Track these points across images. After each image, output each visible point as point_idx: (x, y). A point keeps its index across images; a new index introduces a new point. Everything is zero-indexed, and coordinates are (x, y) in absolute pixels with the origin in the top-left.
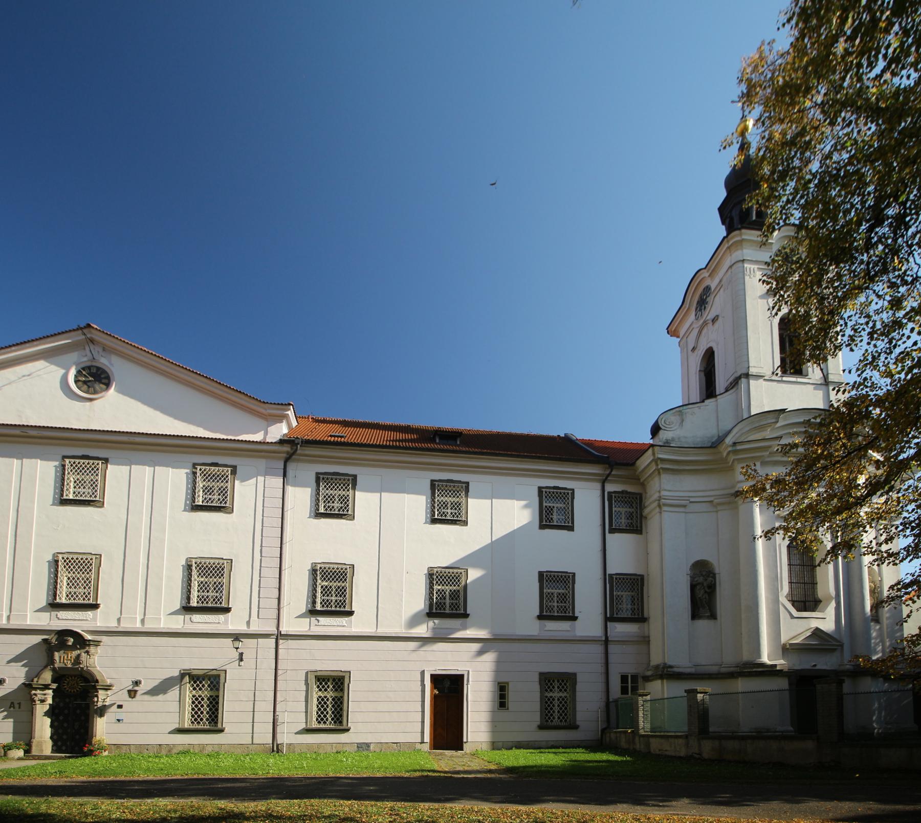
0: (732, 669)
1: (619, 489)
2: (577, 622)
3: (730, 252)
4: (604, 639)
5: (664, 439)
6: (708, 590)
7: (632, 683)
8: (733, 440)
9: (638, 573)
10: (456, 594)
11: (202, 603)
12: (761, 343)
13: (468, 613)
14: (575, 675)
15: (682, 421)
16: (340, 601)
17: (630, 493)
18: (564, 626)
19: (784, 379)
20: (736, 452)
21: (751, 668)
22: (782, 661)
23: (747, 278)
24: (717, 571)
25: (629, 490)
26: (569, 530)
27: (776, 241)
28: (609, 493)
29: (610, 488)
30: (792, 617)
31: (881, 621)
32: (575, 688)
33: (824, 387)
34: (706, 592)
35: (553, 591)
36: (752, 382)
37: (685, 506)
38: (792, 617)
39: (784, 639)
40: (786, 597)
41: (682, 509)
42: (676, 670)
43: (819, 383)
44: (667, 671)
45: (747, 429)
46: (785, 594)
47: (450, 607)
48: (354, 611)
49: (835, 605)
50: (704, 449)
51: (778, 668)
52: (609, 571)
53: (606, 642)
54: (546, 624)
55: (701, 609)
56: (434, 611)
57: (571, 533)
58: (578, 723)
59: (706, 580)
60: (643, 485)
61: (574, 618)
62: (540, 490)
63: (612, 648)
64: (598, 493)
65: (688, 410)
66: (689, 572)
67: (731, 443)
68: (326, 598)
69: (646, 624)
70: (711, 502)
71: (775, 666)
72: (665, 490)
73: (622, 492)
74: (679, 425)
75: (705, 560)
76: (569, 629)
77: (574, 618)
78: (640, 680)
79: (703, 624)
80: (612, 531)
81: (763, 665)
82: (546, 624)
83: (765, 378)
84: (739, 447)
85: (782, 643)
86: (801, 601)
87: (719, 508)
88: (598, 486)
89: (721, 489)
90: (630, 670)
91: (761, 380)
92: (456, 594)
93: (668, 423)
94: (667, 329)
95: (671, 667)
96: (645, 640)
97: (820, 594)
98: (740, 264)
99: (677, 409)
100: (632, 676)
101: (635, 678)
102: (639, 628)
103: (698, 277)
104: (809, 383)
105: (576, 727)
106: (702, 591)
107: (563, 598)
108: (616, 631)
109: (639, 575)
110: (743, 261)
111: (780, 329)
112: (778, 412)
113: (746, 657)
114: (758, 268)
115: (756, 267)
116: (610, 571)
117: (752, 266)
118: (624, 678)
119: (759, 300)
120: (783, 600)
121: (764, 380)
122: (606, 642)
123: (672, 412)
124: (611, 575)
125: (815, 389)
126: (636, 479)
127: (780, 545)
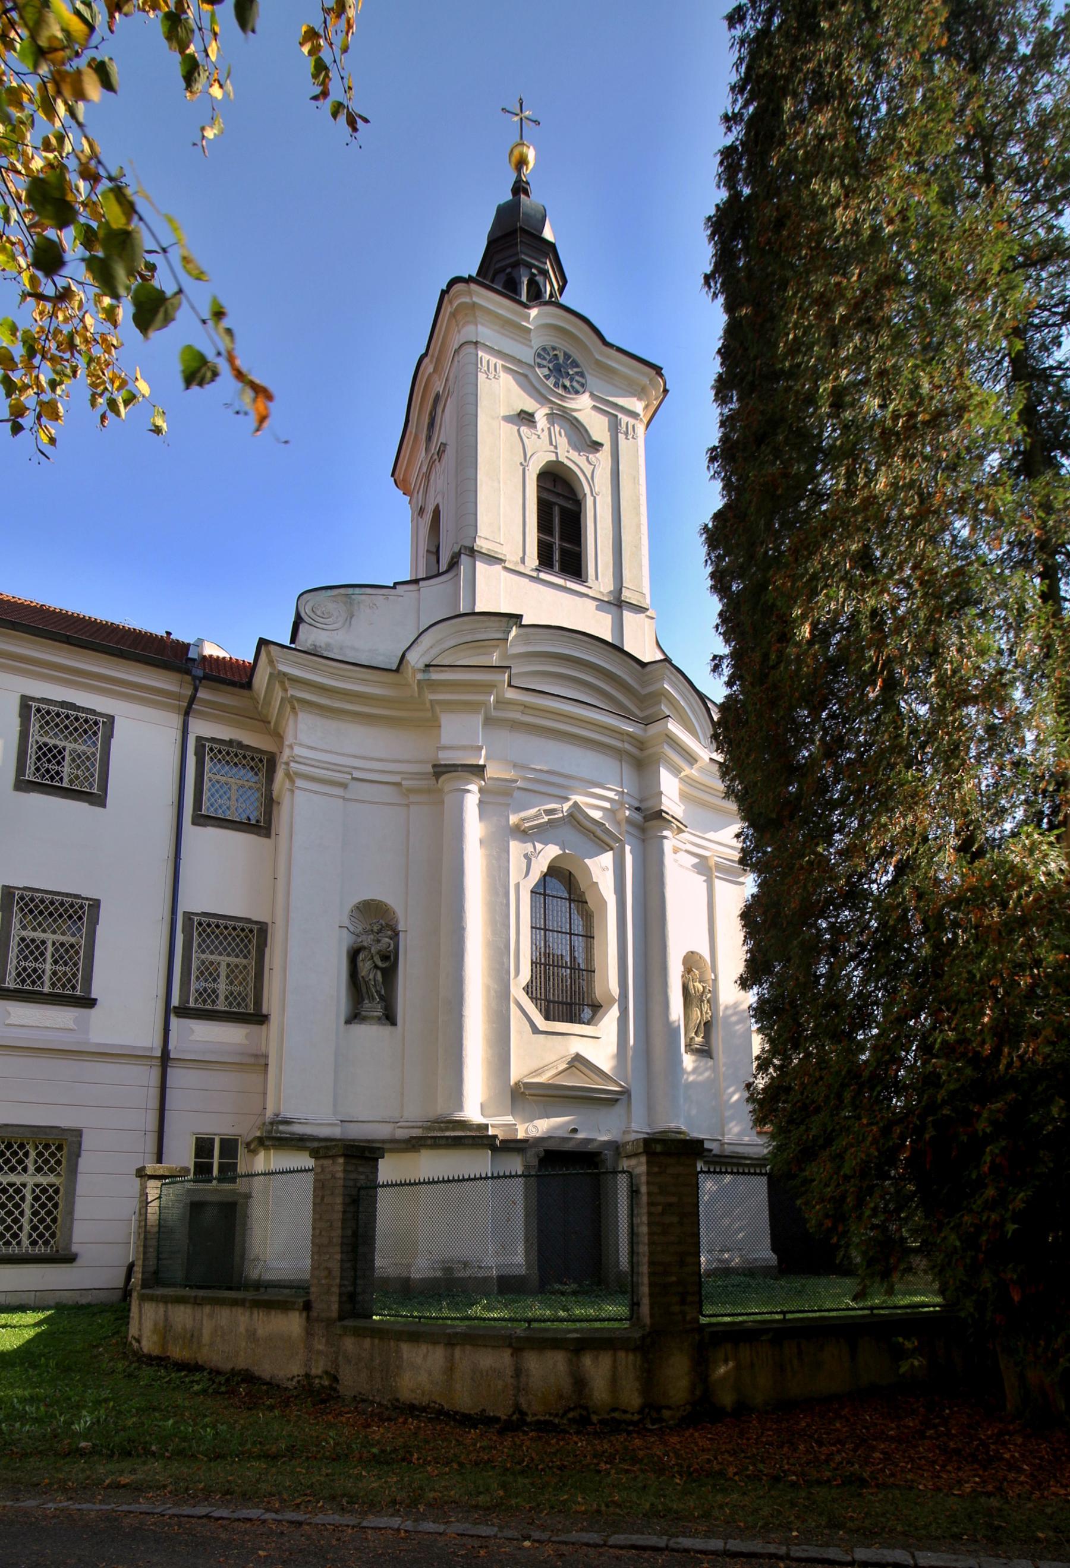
0: (417, 1133)
1: (226, 737)
2: (93, 1012)
3: (457, 325)
4: (159, 1054)
5: (310, 642)
6: (380, 964)
7: (221, 1157)
8: (426, 660)
9: (255, 919)
10: (37, 947)
11: (205, 1001)
12: (502, 500)
13: (93, 996)
14: (78, 1133)
15: (352, 616)
16: (65, 974)
17: (248, 747)
18: (61, 1017)
19: (542, 576)
20: (433, 685)
21: (441, 1130)
22: (510, 1118)
23: (481, 377)
24: (401, 927)
25: (246, 742)
26: (92, 803)
27: (537, 328)
28: (199, 739)
29: (200, 728)
30: (535, 1030)
31: (714, 1055)
32: (76, 1165)
33: (614, 609)
34: (376, 967)
35: (43, 936)
36: (480, 566)
37: (344, 786)
38: (535, 1030)
39: (517, 1073)
40: (527, 989)
41: (338, 791)
42: (298, 1129)
43: (606, 599)
44: (277, 1131)
45: (453, 643)
46: (524, 984)
47: (227, 998)
48: (96, 1000)
49: (618, 1014)
50: (385, 673)
51: (491, 1132)
52: (183, 907)
53: (165, 1059)
54: (193, 1026)
55: (366, 1001)
56: (192, 1004)
57: (98, 810)
58: (75, 1248)
59: (378, 941)
60: (278, 736)
61: (90, 1003)
62: (25, 704)
63: (175, 1075)
64: (173, 734)
65: (363, 597)
66: (346, 922)
67: (421, 665)
68: (30, 964)
69: (264, 1027)
70: (398, 784)
71: (486, 1127)
72: (301, 745)
73: (231, 742)
74: (344, 624)
75: (372, 900)
76: (72, 1026)
77: (90, 1003)
78: (241, 1150)
79: (369, 1033)
80: (201, 819)
81: (463, 1124)
82: (193, 1026)
83: (507, 565)
84: (436, 676)
85: (512, 1083)
86: (562, 1003)
87: (413, 798)
88: (176, 720)
89: (416, 762)
90: (218, 1127)
91: (498, 568)
92: (37, 947)
93: (319, 613)
94: (393, 475)
95: (287, 1122)
96: (258, 1063)
97: (599, 994)
98: (470, 349)
99: (342, 591)
100: (222, 1141)
101: (229, 1147)
102: (247, 1036)
103: (423, 374)
104: (587, 596)
105: (70, 1259)
106: (368, 964)
107: (65, 953)
108: (192, 1038)
109: (257, 923)
110: (476, 343)
111: (540, 488)
112: (505, 619)
113: (440, 1108)
114: (503, 366)
115: (500, 363)
116: (189, 903)
117: (493, 360)
118: (203, 1147)
119: (503, 423)
120: (517, 991)
121: (505, 568)
122: (165, 1059)
123: (330, 593)
124: (188, 916)
125: (598, 608)
126: (261, 721)
127: (518, 885)
